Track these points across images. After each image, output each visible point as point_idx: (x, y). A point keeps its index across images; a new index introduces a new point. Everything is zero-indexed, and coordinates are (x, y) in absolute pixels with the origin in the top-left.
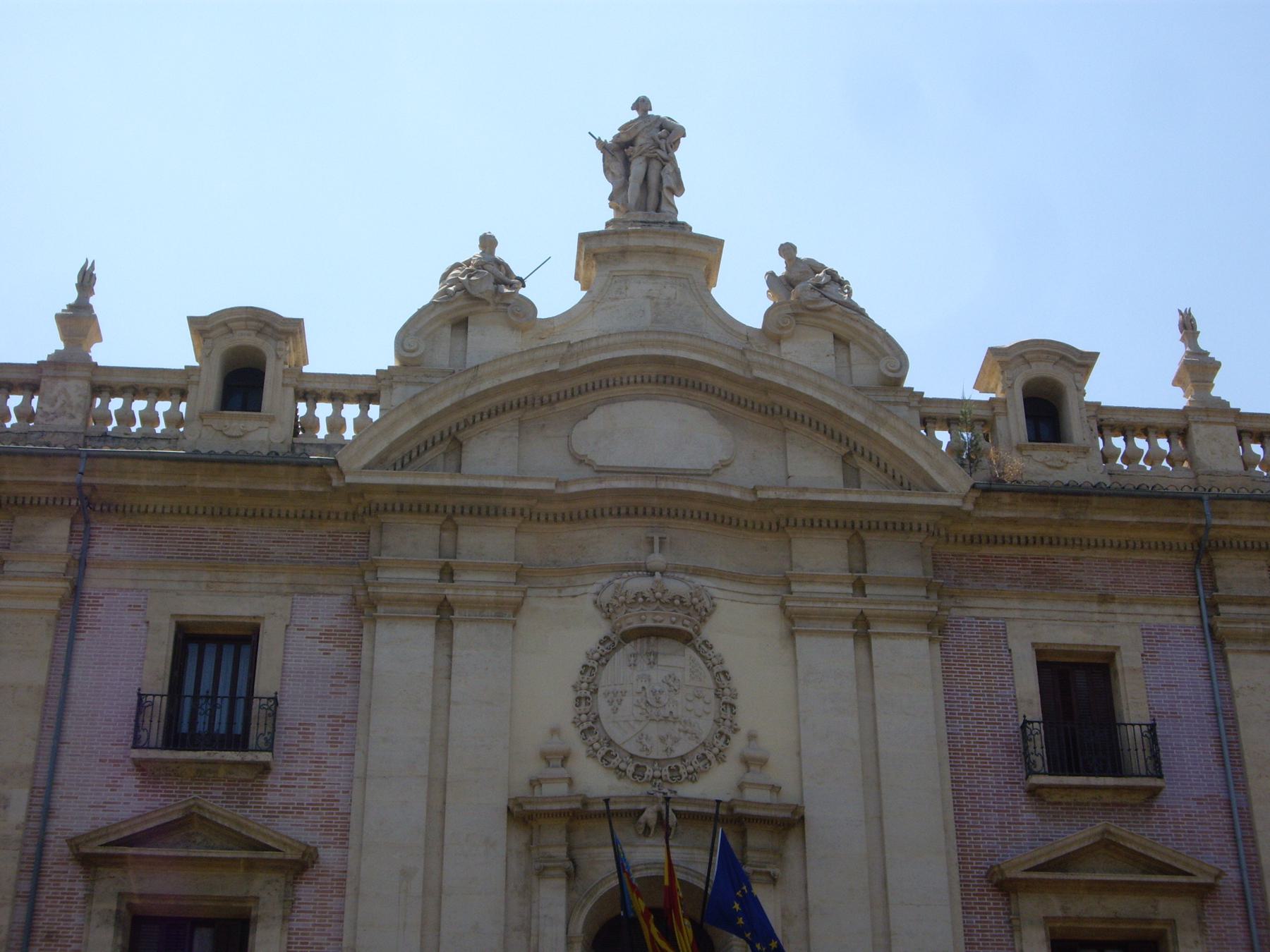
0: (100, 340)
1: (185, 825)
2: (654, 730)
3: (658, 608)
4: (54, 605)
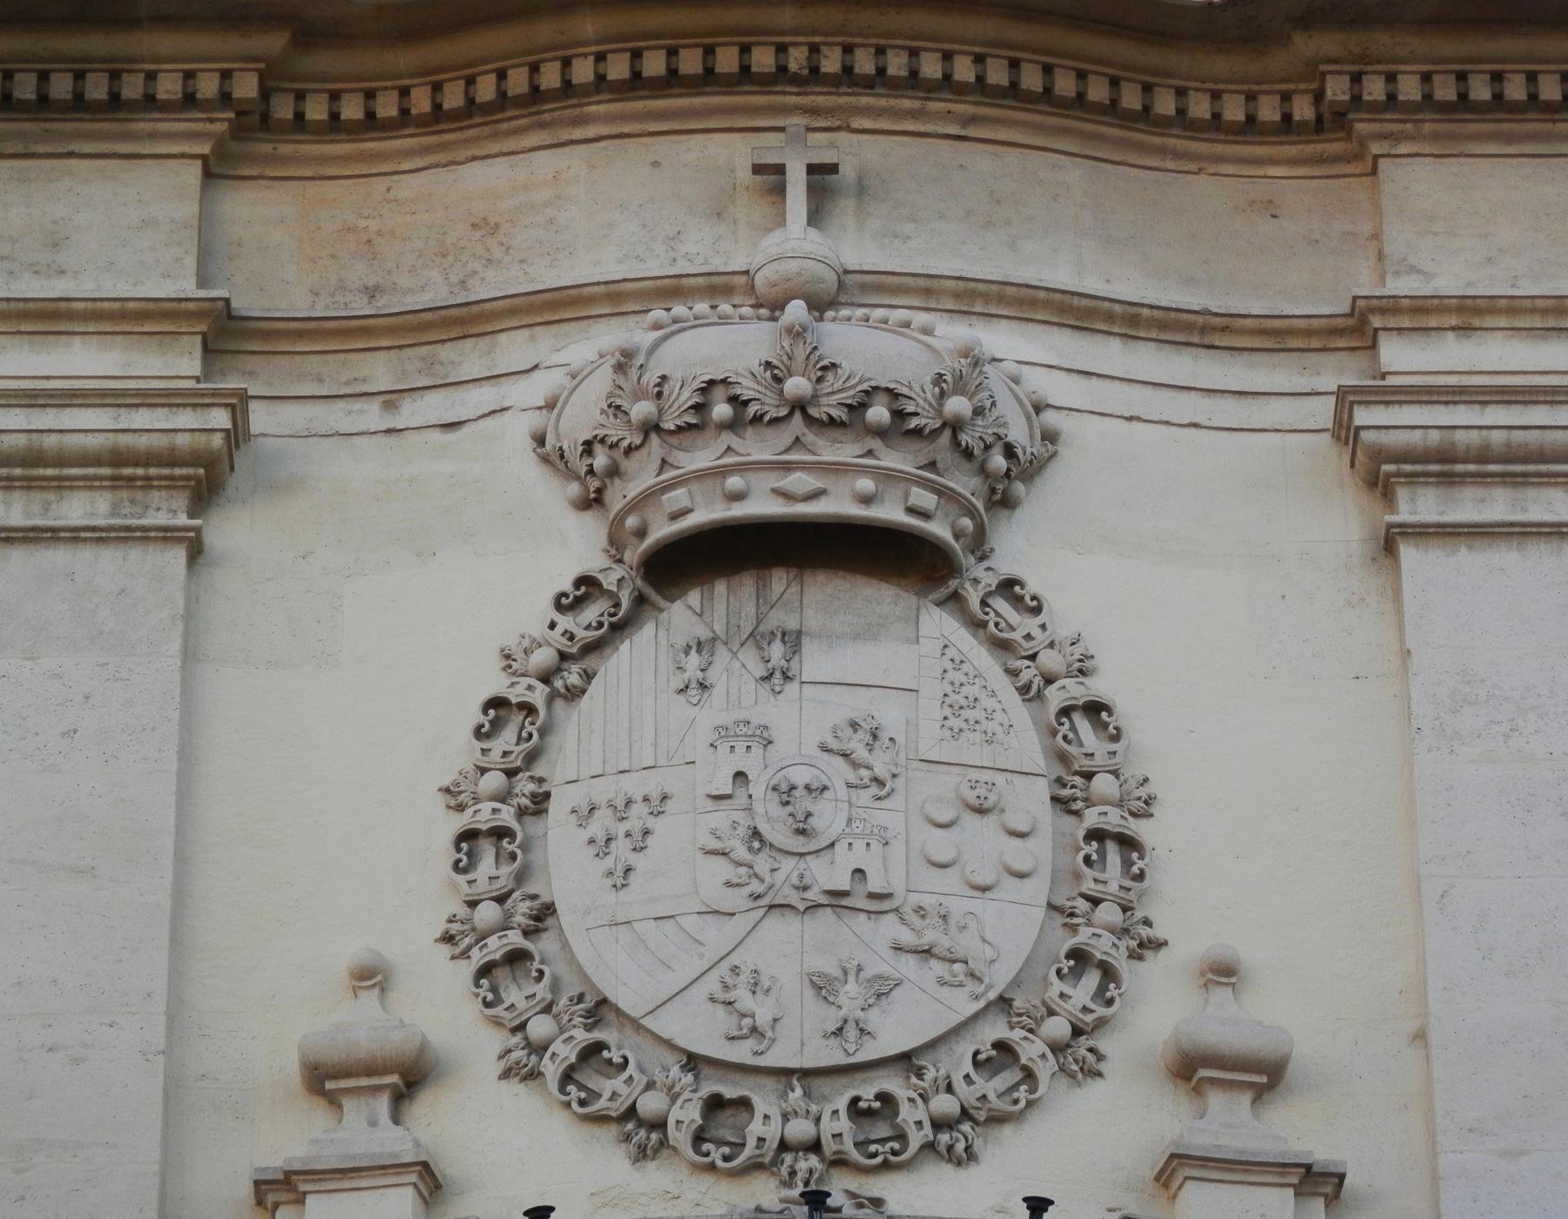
2: (784, 950)
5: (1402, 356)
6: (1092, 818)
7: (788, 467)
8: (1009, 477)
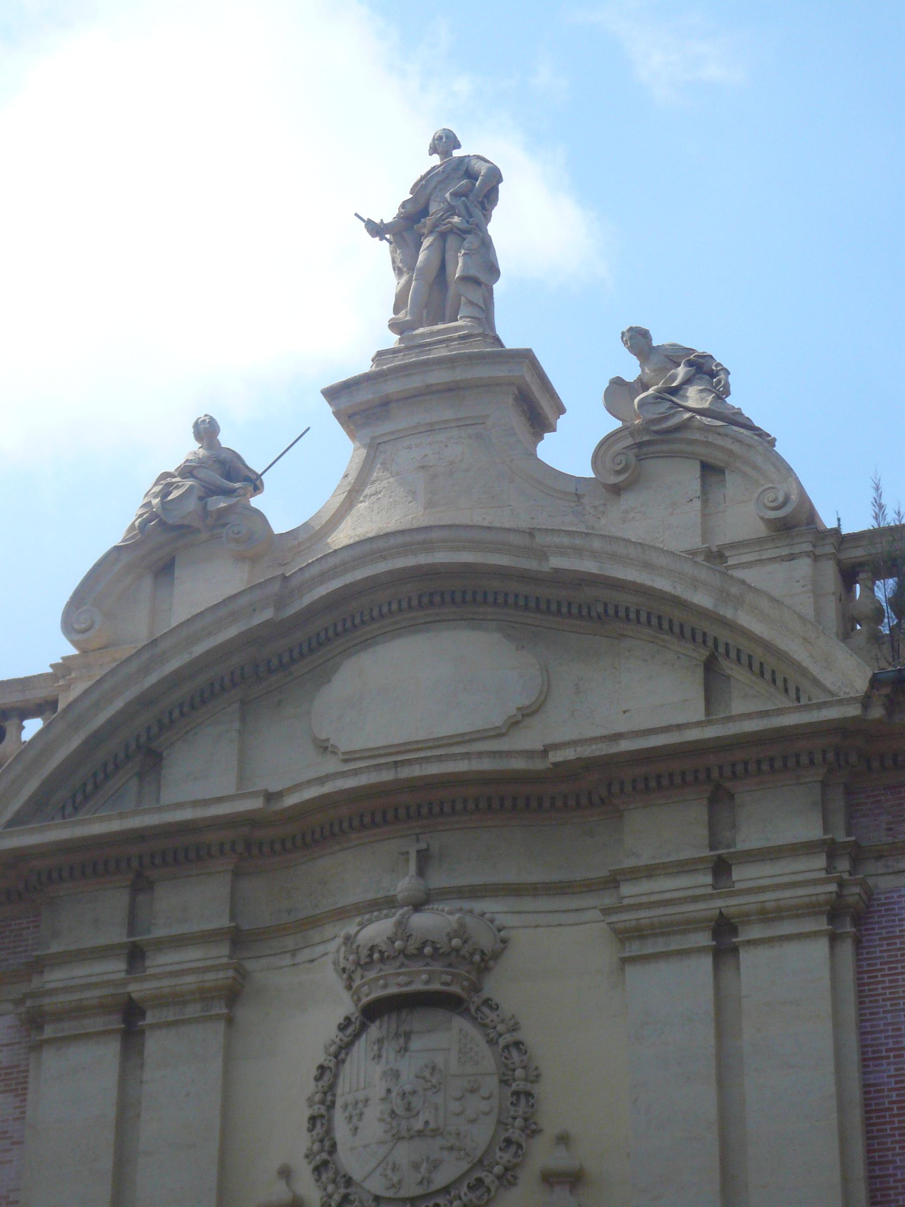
2: (403, 1153)
3: (402, 965)
5: (627, 889)
6: (514, 1087)
7: (399, 974)
8: (485, 962)
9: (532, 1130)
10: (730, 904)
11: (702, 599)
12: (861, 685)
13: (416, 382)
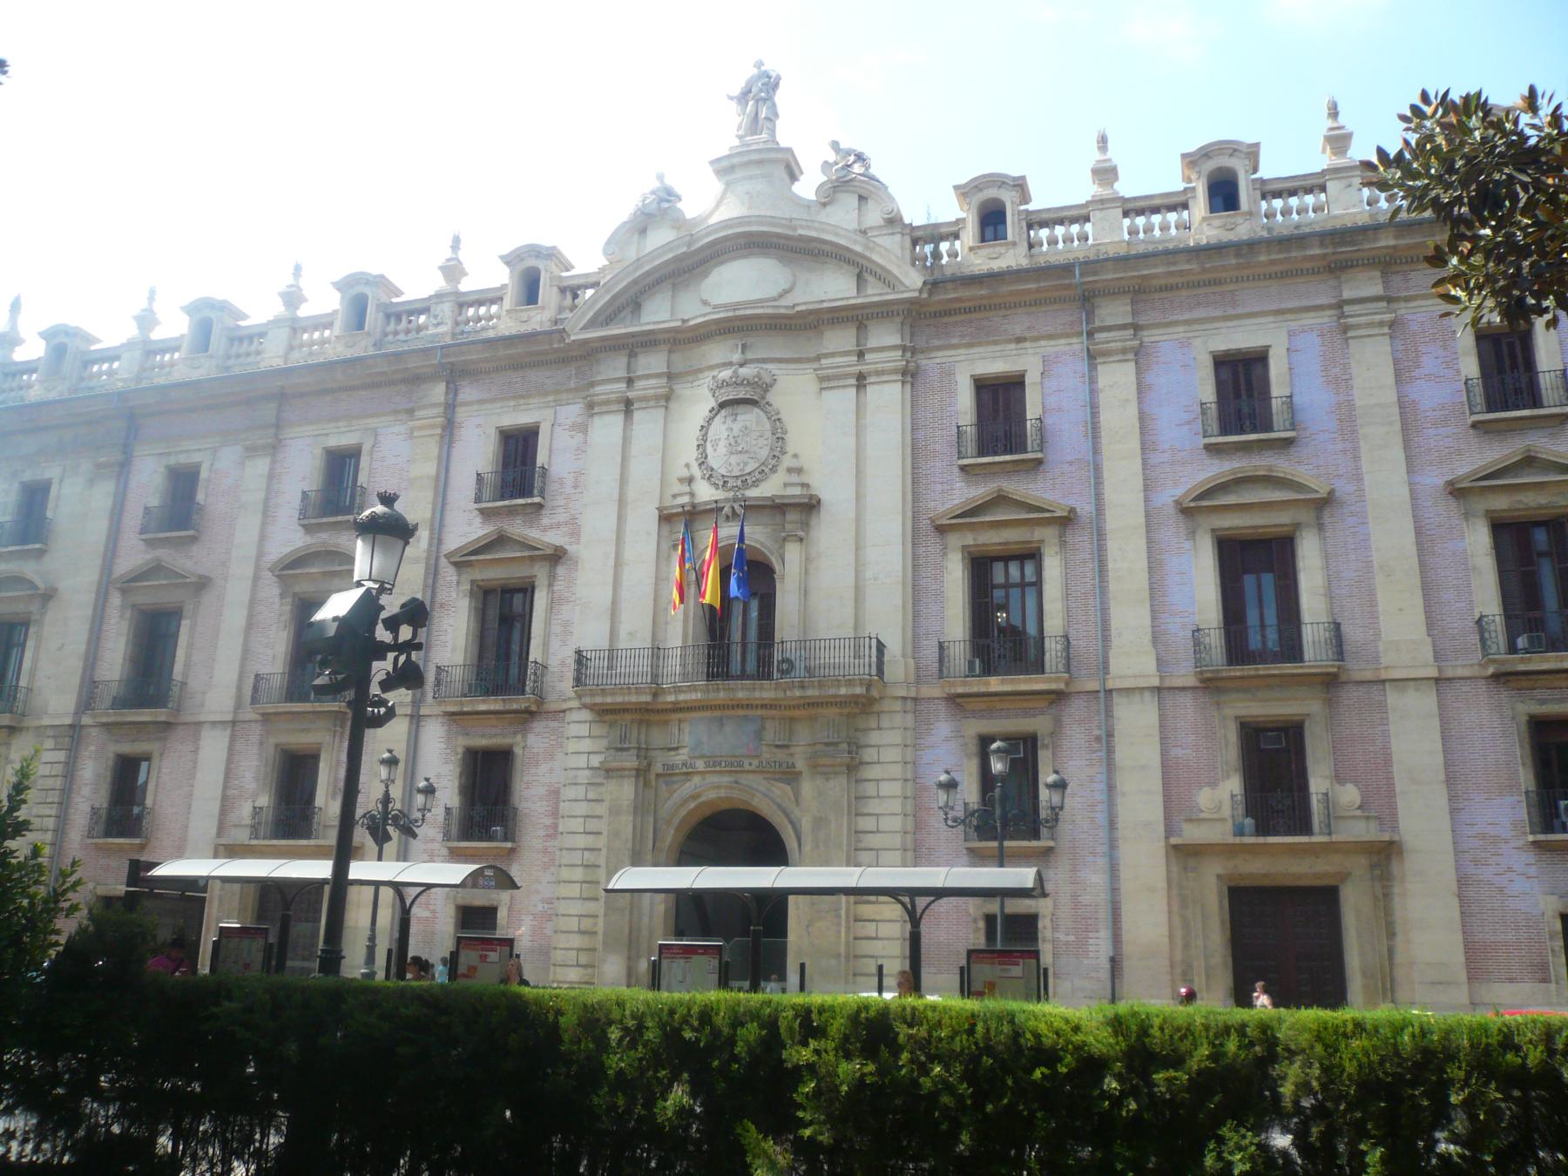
0: (466, 274)
1: (500, 541)
2: (734, 459)
4: (439, 431)
8: (767, 388)
9: (784, 453)
10: (864, 368)
11: (858, 248)
12: (919, 284)
13: (746, 159)
